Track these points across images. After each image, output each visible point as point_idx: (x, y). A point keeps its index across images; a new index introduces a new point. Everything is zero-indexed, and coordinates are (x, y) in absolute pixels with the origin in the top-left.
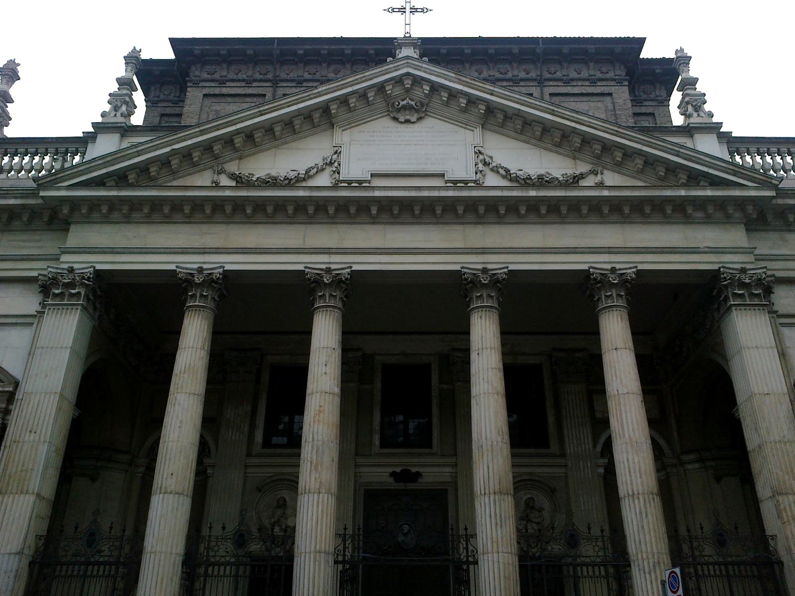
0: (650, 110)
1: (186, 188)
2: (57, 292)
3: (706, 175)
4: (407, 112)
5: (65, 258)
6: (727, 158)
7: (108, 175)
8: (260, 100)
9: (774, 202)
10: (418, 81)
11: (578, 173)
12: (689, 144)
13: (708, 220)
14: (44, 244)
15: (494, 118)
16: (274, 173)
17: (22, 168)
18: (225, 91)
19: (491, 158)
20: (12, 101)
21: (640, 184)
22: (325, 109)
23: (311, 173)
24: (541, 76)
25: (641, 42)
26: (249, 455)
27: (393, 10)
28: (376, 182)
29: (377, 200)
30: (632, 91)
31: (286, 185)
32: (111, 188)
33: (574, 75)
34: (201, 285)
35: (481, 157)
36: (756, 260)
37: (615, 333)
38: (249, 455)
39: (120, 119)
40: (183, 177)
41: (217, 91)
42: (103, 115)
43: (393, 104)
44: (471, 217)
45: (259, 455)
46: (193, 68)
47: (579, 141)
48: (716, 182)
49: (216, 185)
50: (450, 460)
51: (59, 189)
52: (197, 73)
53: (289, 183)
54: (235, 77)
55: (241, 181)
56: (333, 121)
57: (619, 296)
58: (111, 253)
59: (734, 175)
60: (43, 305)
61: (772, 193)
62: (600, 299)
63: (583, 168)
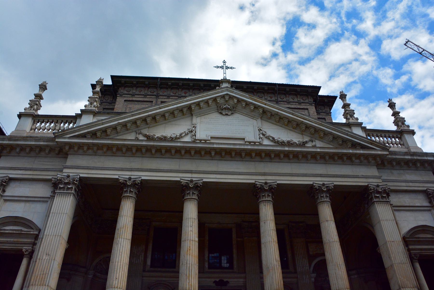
0: (323, 117)
1: (125, 140)
2: (61, 186)
3: (359, 144)
4: (227, 111)
5: (65, 170)
6: (365, 137)
7: (88, 133)
8: (149, 104)
9: (388, 157)
10: (231, 97)
11: (304, 141)
12: (349, 130)
13: (361, 164)
14: (55, 163)
15: (266, 115)
16: (164, 135)
17: (41, 128)
18: (134, 99)
19: (266, 132)
20: (42, 99)
21: (331, 147)
22: (189, 107)
23: (182, 135)
24: (277, 99)
25: (319, 88)
26: (144, 271)
27: (218, 67)
28: (213, 141)
29: (214, 149)
30: (316, 108)
31: (170, 141)
32: (88, 139)
33: (291, 100)
34: (130, 186)
35: (261, 132)
36: (383, 181)
37: (326, 212)
38: (144, 271)
39: (32, 111)
40: (122, 135)
41: (131, 99)
42: (85, 106)
43: (220, 106)
44: (258, 158)
45: (148, 271)
46: (120, 89)
47: (305, 127)
48: (363, 147)
49: (137, 139)
50: (243, 275)
51: (65, 138)
52: (122, 91)
53: (172, 139)
54: (139, 93)
55: (149, 138)
56: (193, 113)
57: (327, 196)
58: (87, 169)
59: (371, 144)
60: (54, 192)
61: (387, 153)
62: (318, 198)
63: (306, 139)
